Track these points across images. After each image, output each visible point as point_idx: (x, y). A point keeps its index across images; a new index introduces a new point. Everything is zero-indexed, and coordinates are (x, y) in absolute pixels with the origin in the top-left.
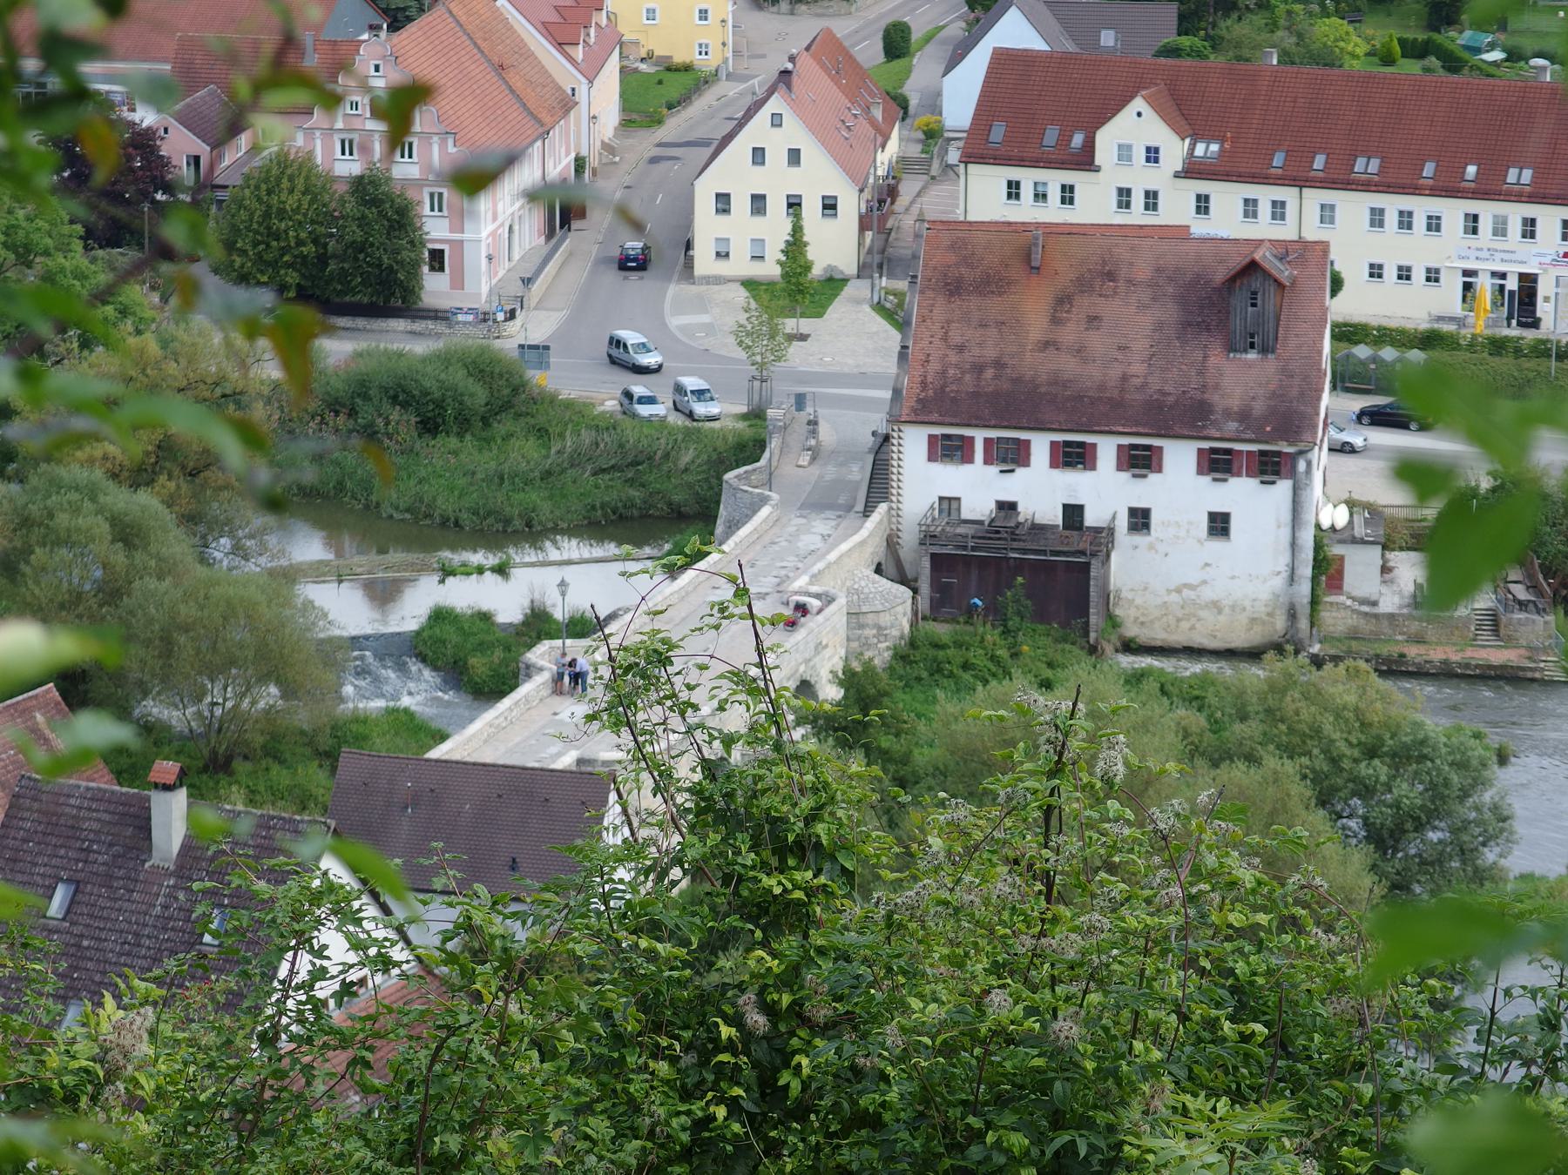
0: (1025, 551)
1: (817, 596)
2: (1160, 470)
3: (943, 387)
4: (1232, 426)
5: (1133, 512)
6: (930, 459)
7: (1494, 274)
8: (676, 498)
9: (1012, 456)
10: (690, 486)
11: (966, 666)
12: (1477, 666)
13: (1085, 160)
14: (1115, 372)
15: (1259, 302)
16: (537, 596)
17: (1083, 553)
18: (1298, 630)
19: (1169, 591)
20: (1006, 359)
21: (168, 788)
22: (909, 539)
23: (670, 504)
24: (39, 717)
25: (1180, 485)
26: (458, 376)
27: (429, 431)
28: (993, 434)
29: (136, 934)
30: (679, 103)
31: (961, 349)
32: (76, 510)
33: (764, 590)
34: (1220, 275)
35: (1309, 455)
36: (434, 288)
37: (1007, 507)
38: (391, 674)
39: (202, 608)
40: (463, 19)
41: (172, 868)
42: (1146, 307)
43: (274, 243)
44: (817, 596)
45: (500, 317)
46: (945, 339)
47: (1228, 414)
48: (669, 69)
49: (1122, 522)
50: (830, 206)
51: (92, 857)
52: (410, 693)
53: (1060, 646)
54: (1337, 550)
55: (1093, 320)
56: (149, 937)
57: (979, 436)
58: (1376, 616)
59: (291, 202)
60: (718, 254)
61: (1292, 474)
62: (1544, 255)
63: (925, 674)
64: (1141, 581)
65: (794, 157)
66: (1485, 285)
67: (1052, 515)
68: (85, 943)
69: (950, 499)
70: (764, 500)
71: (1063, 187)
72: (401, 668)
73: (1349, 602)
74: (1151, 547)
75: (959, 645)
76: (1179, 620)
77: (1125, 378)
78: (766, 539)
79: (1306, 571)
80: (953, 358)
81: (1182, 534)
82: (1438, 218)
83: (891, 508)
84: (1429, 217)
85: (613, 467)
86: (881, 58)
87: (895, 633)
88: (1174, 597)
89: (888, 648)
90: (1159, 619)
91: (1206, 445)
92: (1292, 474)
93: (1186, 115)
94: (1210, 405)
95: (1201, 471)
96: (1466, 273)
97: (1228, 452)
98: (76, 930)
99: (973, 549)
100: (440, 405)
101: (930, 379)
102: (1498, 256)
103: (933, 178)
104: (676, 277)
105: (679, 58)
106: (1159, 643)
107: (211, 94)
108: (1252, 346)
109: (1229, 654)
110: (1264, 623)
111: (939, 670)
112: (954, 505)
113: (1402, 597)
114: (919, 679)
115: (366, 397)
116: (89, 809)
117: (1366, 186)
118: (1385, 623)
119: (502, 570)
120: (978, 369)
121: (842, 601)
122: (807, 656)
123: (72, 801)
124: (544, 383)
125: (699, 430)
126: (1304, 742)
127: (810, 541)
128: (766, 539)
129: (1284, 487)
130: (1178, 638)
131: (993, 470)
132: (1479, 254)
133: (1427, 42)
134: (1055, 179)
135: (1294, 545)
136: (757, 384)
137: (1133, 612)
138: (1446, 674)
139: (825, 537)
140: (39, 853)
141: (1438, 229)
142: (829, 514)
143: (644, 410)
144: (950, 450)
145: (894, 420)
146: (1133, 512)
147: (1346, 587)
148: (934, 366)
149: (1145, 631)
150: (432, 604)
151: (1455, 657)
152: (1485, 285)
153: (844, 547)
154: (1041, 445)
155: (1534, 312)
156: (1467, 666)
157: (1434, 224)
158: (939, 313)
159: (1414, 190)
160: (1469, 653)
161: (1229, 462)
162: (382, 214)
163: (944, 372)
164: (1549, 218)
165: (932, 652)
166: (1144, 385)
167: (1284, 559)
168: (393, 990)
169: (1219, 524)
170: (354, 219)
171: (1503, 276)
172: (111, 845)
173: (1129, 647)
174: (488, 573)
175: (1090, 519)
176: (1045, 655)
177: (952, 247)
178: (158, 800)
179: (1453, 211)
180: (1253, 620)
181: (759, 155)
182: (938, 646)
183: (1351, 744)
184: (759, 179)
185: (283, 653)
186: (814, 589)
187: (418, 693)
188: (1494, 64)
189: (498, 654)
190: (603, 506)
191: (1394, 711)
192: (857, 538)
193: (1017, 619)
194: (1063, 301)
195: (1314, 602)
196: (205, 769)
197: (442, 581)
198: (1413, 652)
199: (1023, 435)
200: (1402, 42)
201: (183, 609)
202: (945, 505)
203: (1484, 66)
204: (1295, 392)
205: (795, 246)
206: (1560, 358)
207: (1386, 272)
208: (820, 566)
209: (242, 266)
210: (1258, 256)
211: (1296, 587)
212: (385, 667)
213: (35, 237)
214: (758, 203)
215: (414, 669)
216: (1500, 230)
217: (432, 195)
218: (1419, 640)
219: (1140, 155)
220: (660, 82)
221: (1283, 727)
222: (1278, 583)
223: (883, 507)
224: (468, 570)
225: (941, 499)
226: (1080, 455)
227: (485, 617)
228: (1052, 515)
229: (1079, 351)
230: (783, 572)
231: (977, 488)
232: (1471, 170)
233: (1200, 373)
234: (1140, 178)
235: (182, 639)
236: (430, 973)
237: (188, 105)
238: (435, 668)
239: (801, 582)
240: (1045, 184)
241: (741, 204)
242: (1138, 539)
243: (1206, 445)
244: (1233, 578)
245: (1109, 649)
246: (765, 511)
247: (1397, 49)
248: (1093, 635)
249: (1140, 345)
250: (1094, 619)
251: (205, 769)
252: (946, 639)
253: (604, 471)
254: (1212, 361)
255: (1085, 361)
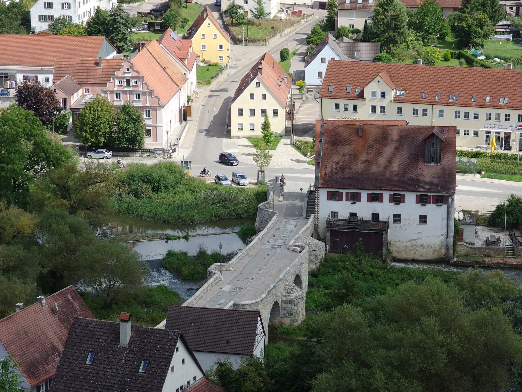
0: (361, 229)
1: (298, 246)
2: (404, 202)
3: (332, 176)
4: (427, 187)
5: (395, 216)
6: (328, 200)
7: (496, 133)
8: (239, 212)
9: (354, 198)
10: (244, 208)
11: (344, 268)
12: (508, 264)
13: (361, 96)
14: (388, 170)
15: (435, 146)
16: (202, 247)
17: (380, 230)
18: (449, 254)
19: (407, 242)
20: (352, 166)
21: (126, 321)
22: (322, 226)
23: (237, 214)
24: (69, 296)
25: (410, 207)
26: (164, 172)
27: (155, 191)
28: (349, 191)
29: (116, 369)
30: (216, 77)
31: (337, 163)
32: (58, 224)
33: (280, 245)
34: (421, 138)
35: (453, 196)
36: (148, 143)
37: (353, 215)
38: (156, 274)
39: (102, 255)
40: (152, 52)
41: (127, 347)
42: (397, 148)
43: (96, 128)
44: (298, 246)
45: (171, 151)
46: (332, 160)
47: (426, 183)
48: (210, 65)
49: (391, 219)
50: (276, 112)
51: (100, 344)
52: (163, 280)
53: (374, 261)
54: (461, 227)
55: (380, 153)
56: (121, 370)
57: (344, 192)
58: (474, 248)
59: (102, 115)
60: (239, 129)
61: (447, 202)
62: (511, 126)
63: (331, 271)
64: (399, 238)
65: (264, 96)
66: (493, 136)
67: (369, 217)
68: (99, 372)
69: (335, 212)
70: (274, 214)
71: (354, 106)
72: (159, 271)
73: (465, 244)
74: (401, 227)
75: (341, 261)
76: (410, 251)
77: (391, 172)
78: (276, 227)
79: (452, 234)
80: (335, 166)
81: (411, 222)
82: (478, 114)
83: (315, 216)
84: (475, 114)
85: (218, 202)
86: (280, 60)
87: (320, 257)
88: (409, 243)
89: (318, 262)
90: (404, 251)
91: (419, 194)
92: (447, 202)
93: (395, 81)
94: (420, 180)
95: (417, 202)
96: (487, 132)
97: (426, 196)
98: (96, 368)
99: (344, 229)
100: (159, 182)
101: (327, 173)
102: (497, 127)
103: (304, 101)
104: (224, 136)
105: (213, 61)
106: (404, 258)
107: (68, 77)
108: (433, 161)
109: (427, 262)
110: (438, 251)
111: (336, 269)
112: (336, 214)
113: (482, 242)
114: (329, 272)
115: (134, 180)
116: (98, 328)
117: (454, 105)
118: (477, 251)
119: (186, 238)
120: (343, 169)
121: (307, 248)
122: (298, 267)
123: (92, 326)
124: (190, 174)
125: (243, 189)
126: (483, 297)
127: (290, 227)
128: (276, 227)
129: (444, 207)
130: (410, 256)
131: (349, 203)
132: (491, 126)
133: (460, 53)
134: (351, 103)
135: (448, 225)
136: (260, 173)
137: (395, 249)
138: (499, 266)
139: (295, 226)
140: (82, 343)
141: (478, 118)
142: (294, 218)
143: (224, 182)
144: (334, 196)
145: (316, 186)
146: (395, 216)
147: (464, 239)
148: (328, 169)
149: (399, 254)
150: (167, 250)
151: (501, 262)
152: (493, 136)
153: (303, 229)
154: (364, 195)
155: (509, 145)
156: (505, 264)
157: (476, 117)
158: (330, 151)
159: (470, 106)
160: (505, 260)
161: (426, 199)
162: (132, 118)
163: (332, 171)
164: (514, 114)
165: (333, 263)
166: (398, 174)
167: (445, 230)
168: (197, 385)
169: (423, 219)
170: (122, 120)
171: (499, 133)
172: (106, 340)
173: (395, 260)
174: (182, 239)
175: (381, 218)
176: (370, 264)
177: (333, 130)
178: (122, 326)
179: (482, 112)
180: (435, 250)
181: (252, 96)
182: (334, 261)
183: (499, 298)
184: (252, 104)
185: (130, 269)
186: (297, 244)
187: (165, 280)
188: (482, 60)
189: (191, 267)
190: (215, 216)
191: (512, 286)
192: (307, 226)
193: (360, 252)
194: (370, 147)
195: (455, 244)
196: (103, 307)
197: (167, 242)
198: (487, 260)
199: (359, 191)
200: (452, 53)
201: (96, 255)
202: (333, 214)
203: (479, 61)
204: (447, 176)
205: (266, 126)
206: (520, 160)
207: (470, 133)
208: (297, 236)
209: (86, 136)
210: (434, 132)
211: (449, 239)
212: (154, 271)
213: (33, 130)
214: (252, 112)
215: (163, 272)
216: (498, 118)
217: (146, 111)
218: (488, 256)
219: (379, 95)
220: (208, 70)
221: (476, 292)
222: (443, 238)
223: (313, 215)
224: (175, 238)
225: (332, 212)
226: (377, 197)
227: (185, 254)
228: (369, 217)
229: (376, 163)
230: (284, 238)
231: (344, 209)
232: (488, 99)
233: (416, 170)
234: (379, 103)
235: (97, 266)
236: (208, 379)
237: (61, 82)
238: (170, 272)
239: (292, 242)
240: (347, 105)
241: (246, 112)
242: (397, 225)
243: (419, 194)
244: (428, 237)
245: (389, 261)
246: (275, 217)
247: (450, 56)
248: (384, 257)
249: (396, 161)
250: (384, 251)
251: (103, 307)
252: (337, 259)
253: (215, 203)
254: (420, 166)
255: (378, 166)
